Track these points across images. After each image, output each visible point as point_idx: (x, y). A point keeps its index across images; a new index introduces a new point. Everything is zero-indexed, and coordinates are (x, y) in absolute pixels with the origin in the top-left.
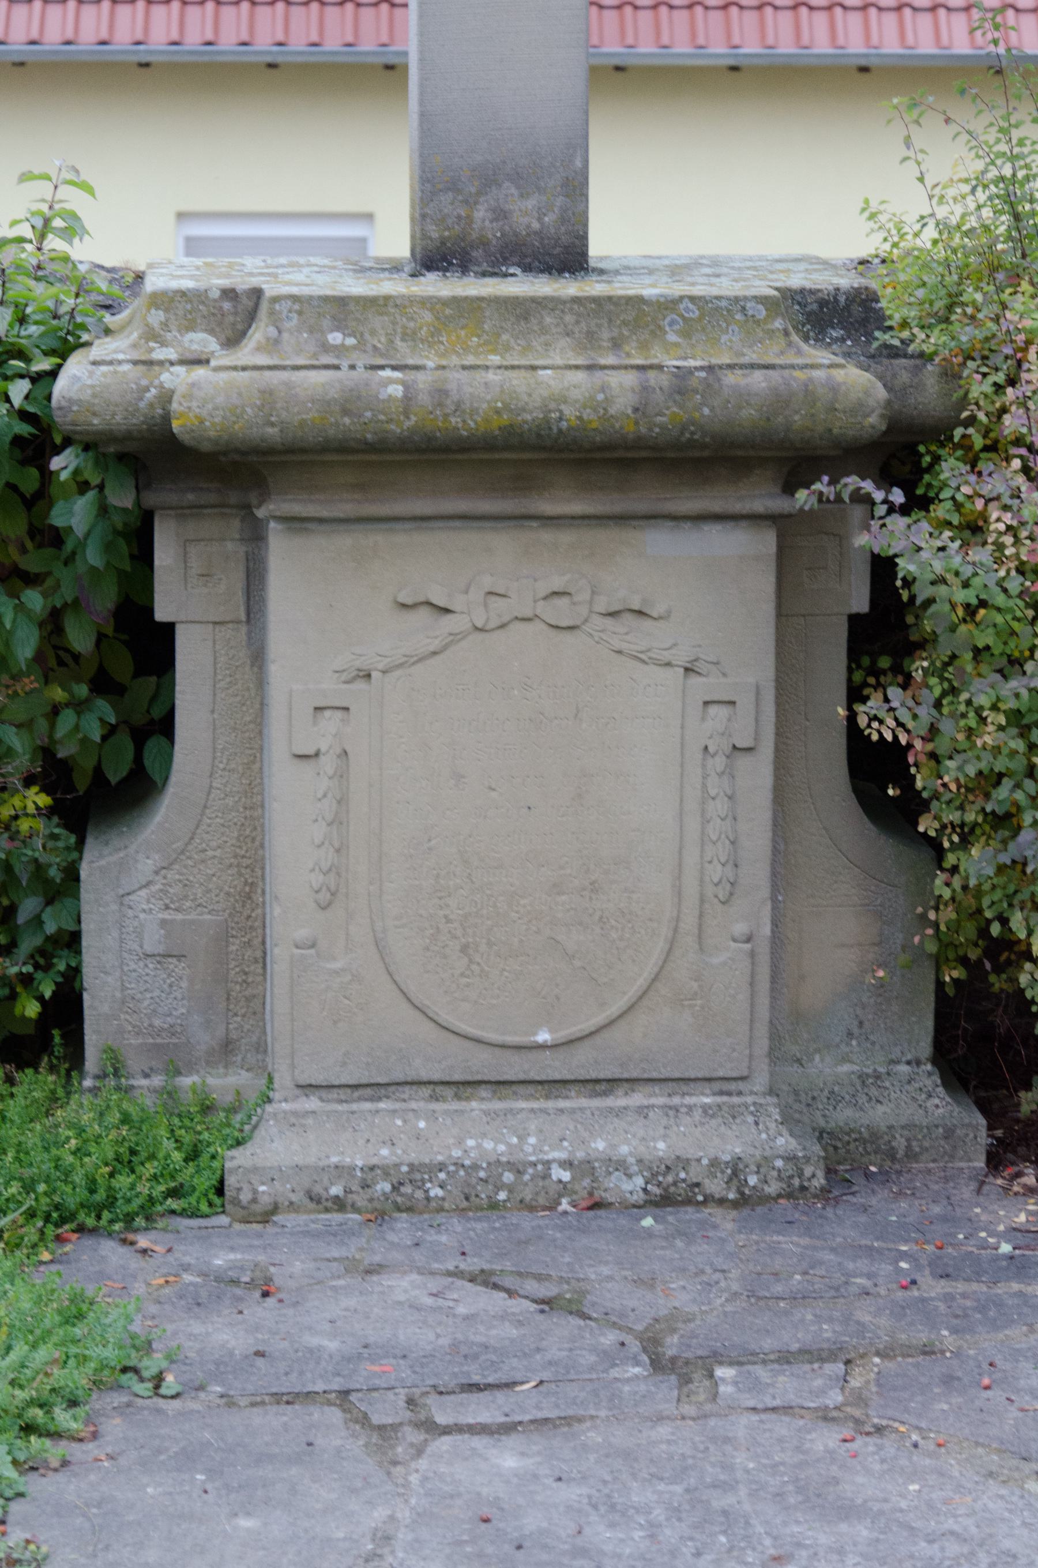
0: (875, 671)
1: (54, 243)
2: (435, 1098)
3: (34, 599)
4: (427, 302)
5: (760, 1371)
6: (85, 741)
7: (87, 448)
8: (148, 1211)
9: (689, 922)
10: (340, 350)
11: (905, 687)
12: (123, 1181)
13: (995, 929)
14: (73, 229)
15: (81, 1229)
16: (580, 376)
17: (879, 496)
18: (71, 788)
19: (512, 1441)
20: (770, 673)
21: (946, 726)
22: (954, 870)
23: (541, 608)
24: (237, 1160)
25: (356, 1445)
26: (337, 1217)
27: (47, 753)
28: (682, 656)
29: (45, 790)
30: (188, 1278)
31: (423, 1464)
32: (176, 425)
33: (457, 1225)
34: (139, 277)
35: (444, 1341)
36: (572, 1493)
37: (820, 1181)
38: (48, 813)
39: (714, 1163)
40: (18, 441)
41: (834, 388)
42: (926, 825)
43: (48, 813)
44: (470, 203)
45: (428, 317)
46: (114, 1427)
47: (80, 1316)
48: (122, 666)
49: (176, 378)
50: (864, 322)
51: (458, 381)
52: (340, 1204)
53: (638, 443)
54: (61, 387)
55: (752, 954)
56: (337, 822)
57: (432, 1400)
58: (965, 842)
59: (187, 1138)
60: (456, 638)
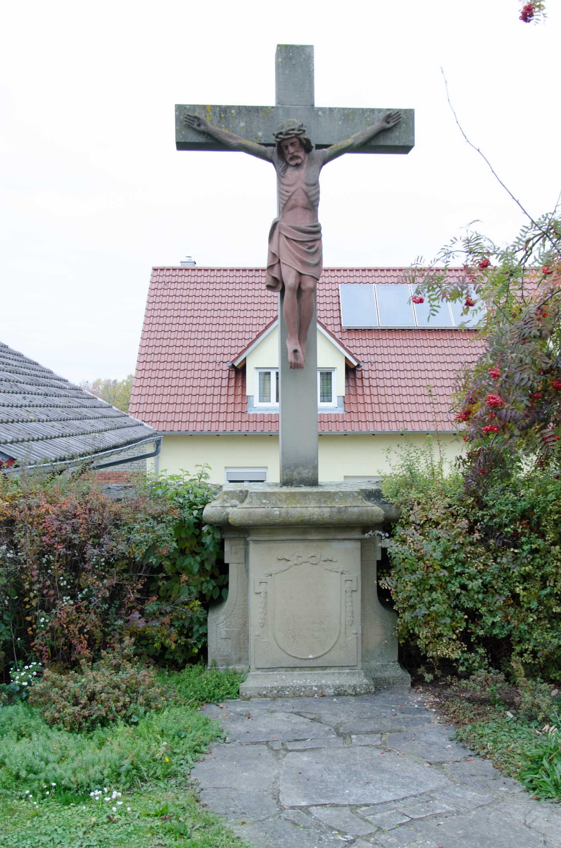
0: (382, 573)
1: (202, 480)
2: (286, 671)
3: (198, 558)
4: (283, 493)
5: (362, 737)
6: (209, 590)
7: (210, 525)
8: (222, 698)
9: (343, 630)
10: (265, 504)
11: (389, 576)
12: (217, 691)
13: (411, 631)
14: (207, 477)
15: (207, 702)
16: (317, 509)
17: (383, 535)
18: (205, 600)
19: (306, 753)
20: (360, 574)
21: (399, 586)
22: (402, 618)
23: (309, 560)
24: (242, 686)
25: (270, 755)
26: (264, 699)
27: (200, 592)
28: (340, 570)
29: (200, 601)
30: (231, 714)
31: (285, 759)
32: (230, 521)
33: (292, 701)
34: (221, 487)
35: (290, 729)
36: (320, 766)
37: (373, 690)
38: (201, 605)
39: (350, 686)
40: (195, 523)
41: (373, 511)
42: (395, 608)
43: (201, 605)
44: (293, 471)
45: (284, 496)
46: (215, 750)
47: (207, 724)
48: (217, 573)
49: (230, 510)
50: (378, 496)
51: (291, 510)
52: (265, 696)
53: (330, 523)
54: (205, 512)
55: (357, 637)
56: (265, 608)
57: (287, 743)
58: (404, 612)
59: (231, 681)
60: (291, 566)
